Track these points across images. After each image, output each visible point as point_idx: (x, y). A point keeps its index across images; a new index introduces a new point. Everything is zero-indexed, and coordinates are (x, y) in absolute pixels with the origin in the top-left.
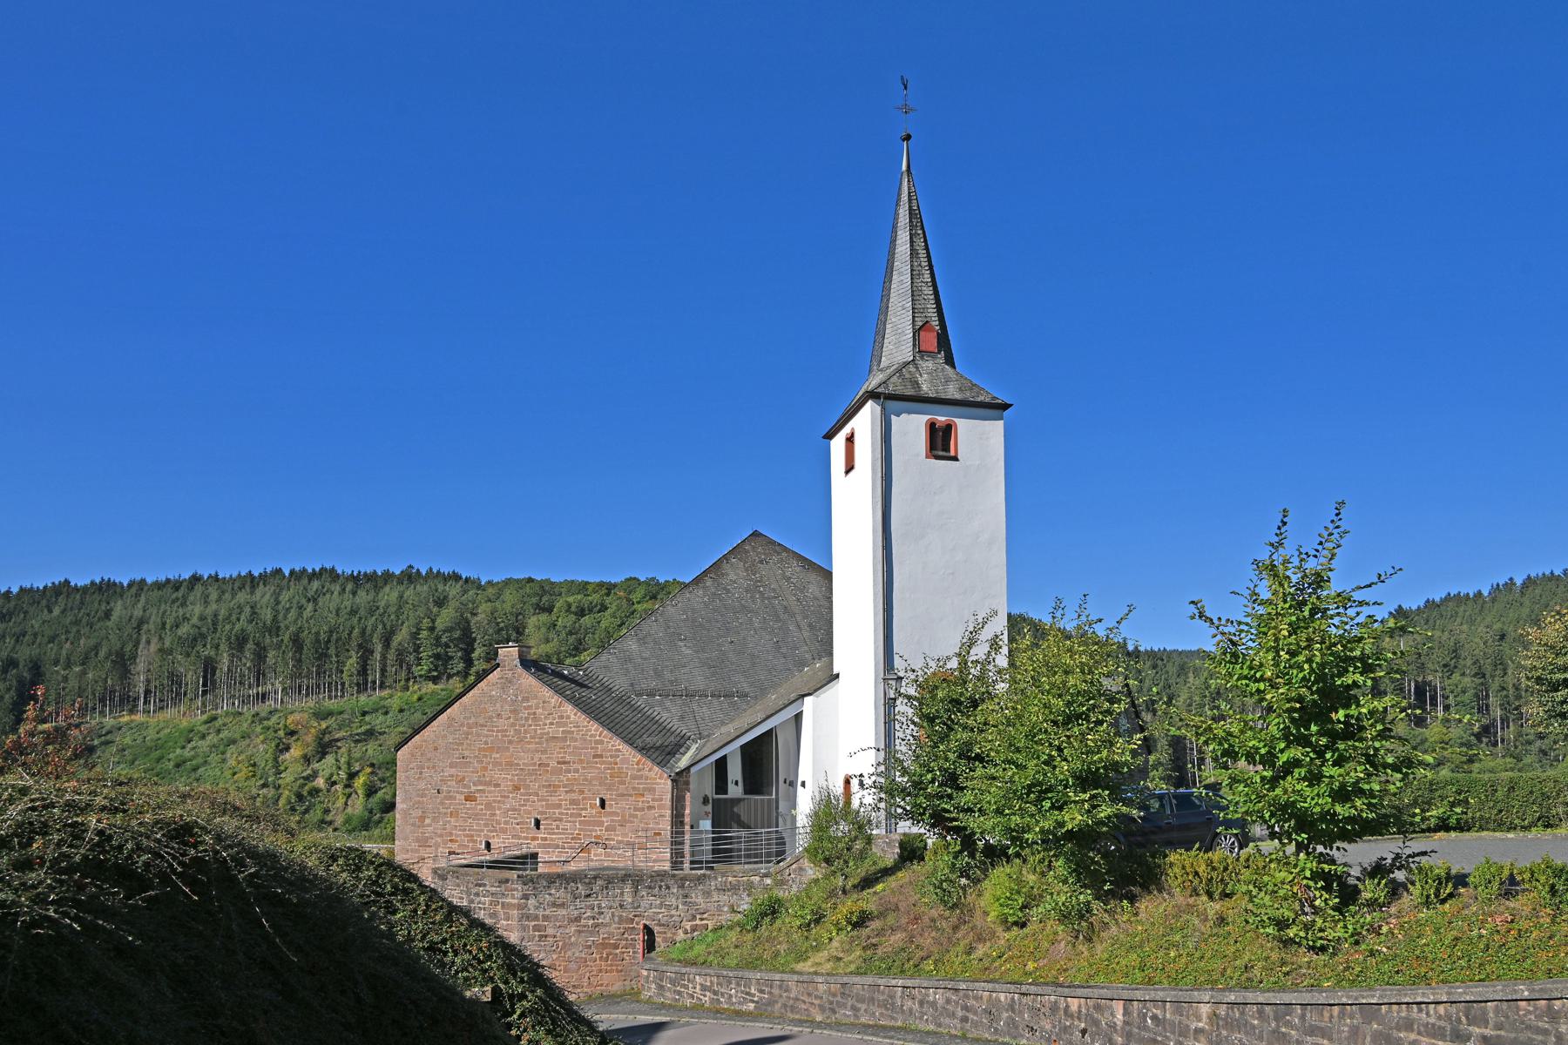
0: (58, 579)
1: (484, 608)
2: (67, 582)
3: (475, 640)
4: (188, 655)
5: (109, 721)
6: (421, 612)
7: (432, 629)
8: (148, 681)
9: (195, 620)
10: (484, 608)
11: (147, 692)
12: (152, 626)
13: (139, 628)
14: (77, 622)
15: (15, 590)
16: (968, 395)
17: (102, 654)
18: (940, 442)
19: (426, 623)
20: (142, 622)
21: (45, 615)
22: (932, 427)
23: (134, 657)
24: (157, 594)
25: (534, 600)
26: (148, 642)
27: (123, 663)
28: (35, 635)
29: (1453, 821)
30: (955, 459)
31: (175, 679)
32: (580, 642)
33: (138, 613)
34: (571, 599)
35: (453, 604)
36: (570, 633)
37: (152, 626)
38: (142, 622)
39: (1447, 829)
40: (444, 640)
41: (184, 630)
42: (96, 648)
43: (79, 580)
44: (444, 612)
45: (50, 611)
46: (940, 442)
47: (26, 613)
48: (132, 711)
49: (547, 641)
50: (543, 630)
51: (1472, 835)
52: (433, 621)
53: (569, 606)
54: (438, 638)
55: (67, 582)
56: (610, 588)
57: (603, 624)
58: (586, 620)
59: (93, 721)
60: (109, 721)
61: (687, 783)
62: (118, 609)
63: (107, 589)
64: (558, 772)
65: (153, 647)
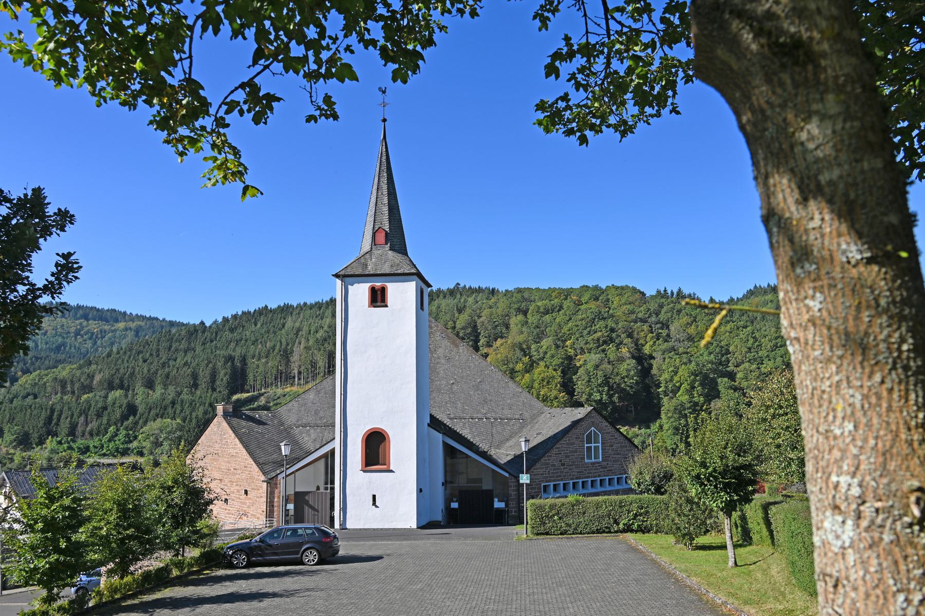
0: (262, 305)
1: (486, 312)
2: (266, 307)
3: (480, 334)
4: (320, 350)
5: (279, 391)
6: (448, 317)
7: (454, 328)
8: (300, 367)
9: (326, 328)
10: (486, 312)
11: (300, 373)
12: (304, 333)
13: (297, 334)
14: (268, 332)
15: (240, 313)
16: (394, 271)
17: (276, 351)
18: (378, 298)
19: (450, 324)
20: (299, 330)
21: (253, 328)
22: (373, 291)
23: (292, 352)
24: (308, 312)
25: (516, 306)
26: (300, 343)
27: (286, 355)
28: (246, 341)
29: (635, 527)
30: (386, 306)
31: (314, 365)
32: (542, 332)
33: (297, 325)
34: (540, 304)
35: (468, 311)
36: (537, 327)
37: (304, 333)
38: (299, 330)
39: (632, 531)
40: (461, 335)
41: (319, 335)
42: (274, 348)
43: (273, 305)
44: (462, 316)
45: (256, 325)
46: (378, 298)
47: (243, 327)
48: (292, 385)
49: (522, 333)
50: (519, 326)
51: (651, 535)
52: (455, 323)
53: (539, 307)
54: (458, 333)
55: (266, 307)
56: (567, 293)
57: (557, 320)
58: (547, 318)
59: (271, 391)
60: (279, 391)
61: (276, 484)
62: (289, 323)
63: (286, 310)
64: (234, 474)
65: (302, 346)
